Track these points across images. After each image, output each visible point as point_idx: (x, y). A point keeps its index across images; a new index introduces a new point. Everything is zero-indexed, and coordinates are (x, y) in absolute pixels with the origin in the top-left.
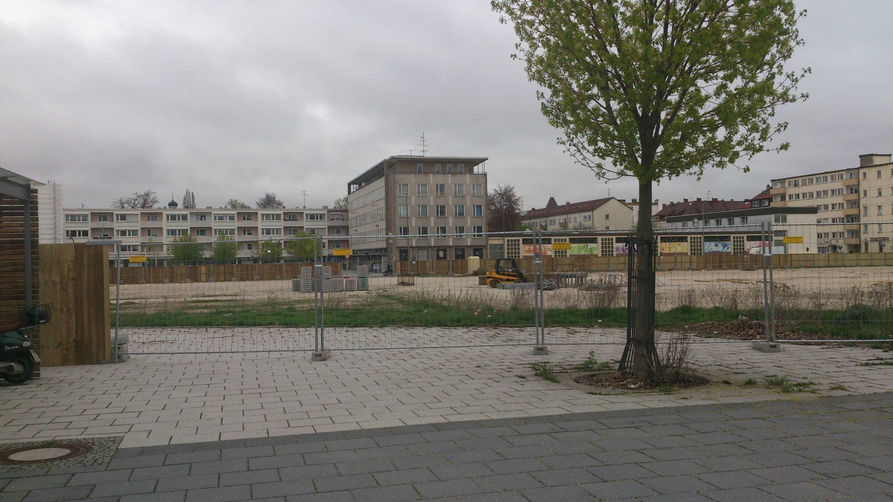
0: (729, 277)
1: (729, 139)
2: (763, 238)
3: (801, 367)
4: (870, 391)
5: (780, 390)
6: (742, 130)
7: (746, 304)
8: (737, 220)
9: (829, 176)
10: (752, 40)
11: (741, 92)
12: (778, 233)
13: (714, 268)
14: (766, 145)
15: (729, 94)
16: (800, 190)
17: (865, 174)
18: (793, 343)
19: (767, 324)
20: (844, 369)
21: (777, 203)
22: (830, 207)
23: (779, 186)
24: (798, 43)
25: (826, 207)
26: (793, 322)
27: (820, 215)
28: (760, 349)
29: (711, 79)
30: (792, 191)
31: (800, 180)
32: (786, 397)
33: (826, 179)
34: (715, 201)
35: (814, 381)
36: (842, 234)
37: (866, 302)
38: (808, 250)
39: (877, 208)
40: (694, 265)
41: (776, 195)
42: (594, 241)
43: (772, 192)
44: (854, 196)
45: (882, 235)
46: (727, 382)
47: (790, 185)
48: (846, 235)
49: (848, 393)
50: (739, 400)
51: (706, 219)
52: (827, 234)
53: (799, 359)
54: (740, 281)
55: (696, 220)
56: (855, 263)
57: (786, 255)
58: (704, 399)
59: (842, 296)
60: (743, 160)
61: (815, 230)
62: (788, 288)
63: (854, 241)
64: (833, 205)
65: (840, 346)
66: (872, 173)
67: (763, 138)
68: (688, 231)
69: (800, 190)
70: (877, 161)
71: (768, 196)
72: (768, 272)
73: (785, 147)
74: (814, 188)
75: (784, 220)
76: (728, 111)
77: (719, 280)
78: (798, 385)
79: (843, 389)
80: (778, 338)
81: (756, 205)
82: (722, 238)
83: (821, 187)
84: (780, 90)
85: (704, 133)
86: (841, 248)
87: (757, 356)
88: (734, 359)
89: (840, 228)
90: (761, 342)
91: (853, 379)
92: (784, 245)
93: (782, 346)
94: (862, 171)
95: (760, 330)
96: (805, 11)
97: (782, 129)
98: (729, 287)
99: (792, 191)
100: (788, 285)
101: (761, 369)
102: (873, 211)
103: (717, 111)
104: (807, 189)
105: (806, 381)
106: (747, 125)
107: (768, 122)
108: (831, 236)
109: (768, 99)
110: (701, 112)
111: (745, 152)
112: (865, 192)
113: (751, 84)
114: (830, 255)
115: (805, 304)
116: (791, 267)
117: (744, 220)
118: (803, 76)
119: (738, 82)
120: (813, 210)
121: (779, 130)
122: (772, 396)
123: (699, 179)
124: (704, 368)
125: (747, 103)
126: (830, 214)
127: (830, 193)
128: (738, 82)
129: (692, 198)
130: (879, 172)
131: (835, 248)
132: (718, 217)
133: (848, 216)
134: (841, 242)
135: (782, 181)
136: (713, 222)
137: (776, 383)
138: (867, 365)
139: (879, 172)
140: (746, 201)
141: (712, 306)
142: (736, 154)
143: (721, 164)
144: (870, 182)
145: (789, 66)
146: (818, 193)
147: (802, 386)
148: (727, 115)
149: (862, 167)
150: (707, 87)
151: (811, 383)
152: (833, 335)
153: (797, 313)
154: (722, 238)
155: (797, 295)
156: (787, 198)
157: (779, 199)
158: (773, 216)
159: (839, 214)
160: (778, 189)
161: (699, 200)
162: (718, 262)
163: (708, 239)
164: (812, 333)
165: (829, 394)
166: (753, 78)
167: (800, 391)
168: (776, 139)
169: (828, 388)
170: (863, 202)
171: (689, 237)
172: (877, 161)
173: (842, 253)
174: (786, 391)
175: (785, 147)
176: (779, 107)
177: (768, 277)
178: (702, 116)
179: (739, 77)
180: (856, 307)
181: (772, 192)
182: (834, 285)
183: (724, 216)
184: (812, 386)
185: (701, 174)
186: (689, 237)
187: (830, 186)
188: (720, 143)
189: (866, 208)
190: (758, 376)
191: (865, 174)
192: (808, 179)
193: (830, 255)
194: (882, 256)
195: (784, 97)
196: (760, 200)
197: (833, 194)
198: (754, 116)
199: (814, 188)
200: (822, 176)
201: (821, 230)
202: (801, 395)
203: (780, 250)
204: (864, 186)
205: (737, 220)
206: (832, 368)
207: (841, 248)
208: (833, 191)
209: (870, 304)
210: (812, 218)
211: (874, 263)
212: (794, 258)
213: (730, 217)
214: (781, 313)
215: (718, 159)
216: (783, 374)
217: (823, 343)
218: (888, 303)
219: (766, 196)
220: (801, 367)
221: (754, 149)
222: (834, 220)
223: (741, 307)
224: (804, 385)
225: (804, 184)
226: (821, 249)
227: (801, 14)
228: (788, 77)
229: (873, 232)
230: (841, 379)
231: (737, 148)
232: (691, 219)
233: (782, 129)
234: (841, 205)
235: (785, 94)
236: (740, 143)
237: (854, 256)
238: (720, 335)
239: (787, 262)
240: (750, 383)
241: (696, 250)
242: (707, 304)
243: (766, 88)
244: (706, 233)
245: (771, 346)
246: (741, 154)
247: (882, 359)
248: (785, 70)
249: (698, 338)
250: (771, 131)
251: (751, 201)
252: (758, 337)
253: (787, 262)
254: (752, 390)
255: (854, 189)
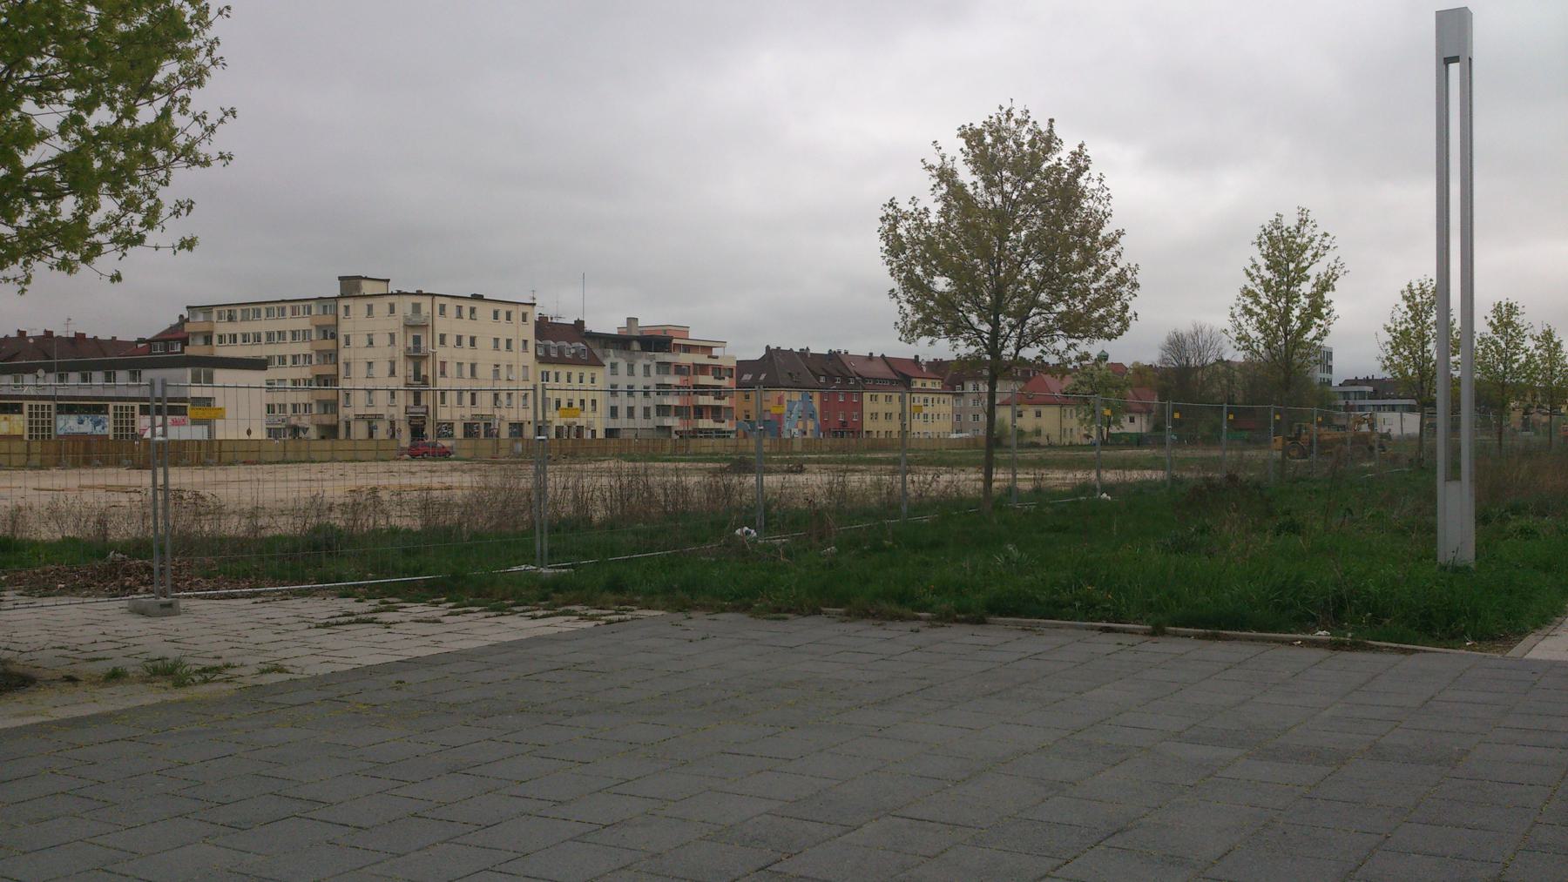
0: (100, 481)
1: (81, 219)
2: (153, 409)
3: (215, 638)
4: (326, 669)
5: (169, 684)
6: (108, 205)
7: (123, 530)
8: (122, 376)
9: (288, 306)
10: (126, 39)
11: (105, 133)
12: (197, 401)
13: (76, 465)
14: (152, 236)
15: (84, 134)
16: (239, 328)
17: (347, 308)
18: (204, 598)
19: (156, 566)
20: (288, 636)
21: (196, 349)
22: (289, 361)
23: (201, 318)
24: (214, 63)
25: (283, 360)
26: (207, 560)
27: (272, 373)
28: (142, 612)
29: (49, 101)
30: (224, 328)
31: (238, 309)
32: (180, 694)
33: (283, 312)
34: (80, 337)
35: (232, 661)
36: (308, 407)
37: (338, 521)
38: (249, 432)
39: (365, 366)
40: (36, 460)
41: (195, 334)
42: (16, 409)
43: (188, 328)
44: (328, 345)
45: (371, 411)
46: (71, 679)
47: (220, 317)
48: (314, 407)
49: (287, 677)
50: (77, 712)
51: (63, 371)
52: (283, 407)
53: (213, 625)
54: (124, 490)
55: (41, 373)
56: (327, 456)
57: (211, 441)
58: (20, 715)
59: (294, 512)
60: (108, 260)
61: (261, 399)
62: (203, 498)
63: (327, 420)
64: (294, 357)
65: (285, 596)
66: (358, 307)
67: (149, 223)
68: (25, 392)
69: (239, 328)
70: (367, 288)
71: (180, 335)
72: (160, 471)
73: (188, 244)
74: (262, 326)
75: (210, 379)
76: (80, 165)
77: (81, 488)
78: (204, 670)
79: (281, 670)
80: (179, 590)
81: (159, 350)
82: (95, 408)
83: (275, 325)
84: (180, 140)
85: (33, 202)
86: (306, 430)
87: (137, 624)
88: (92, 632)
89: (303, 397)
90: (143, 598)
91: (298, 652)
92: (207, 422)
93: (183, 604)
94: (342, 303)
95: (146, 578)
96: (228, 8)
97: (183, 212)
98: (103, 499)
99: (224, 328)
100: (202, 493)
101: (140, 649)
102: (359, 370)
103: (61, 162)
104: (251, 327)
105: (219, 663)
106: (117, 196)
107: (159, 195)
108: (289, 409)
109: (160, 155)
110: (27, 160)
111: (112, 246)
112: (347, 338)
113: (126, 123)
114: (287, 442)
115: (234, 526)
116: (220, 463)
117: (135, 376)
118: (222, 121)
119: (102, 116)
120: (260, 364)
121: (177, 213)
122: (150, 696)
123: (23, 291)
124: (26, 656)
125: (121, 156)
126: (289, 373)
127: (289, 337)
128: (102, 116)
129: (35, 330)
130: (370, 307)
131: (295, 430)
132: (85, 370)
133: (318, 377)
134: (305, 421)
135: (207, 309)
136: (74, 378)
137: (166, 672)
138: (326, 625)
139: (370, 307)
140: (141, 341)
141: (59, 536)
142: (96, 249)
143: (65, 265)
144: (355, 321)
145: (200, 99)
146: (270, 336)
147: (209, 673)
148: (76, 173)
149: (342, 297)
150: (48, 117)
151: (228, 666)
152: (278, 579)
153: (217, 544)
154: (95, 408)
155: (218, 511)
156: (215, 340)
157: (200, 342)
158: (189, 372)
159: (305, 373)
160: (198, 323)
161: (49, 334)
162: (85, 453)
163: (69, 410)
164: (236, 578)
165: (256, 682)
166: (129, 112)
167: (206, 681)
168: (170, 230)
169: (255, 671)
170: (344, 354)
171: (26, 404)
172: (367, 288)
173: (308, 440)
174: (180, 683)
175: (188, 244)
176: (180, 172)
177: (160, 481)
178: (30, 169)
179: (104, 107)
180: (317, 529)
181: (188, 328)
182: (279, 494)
183: (98, 366)
184: (231, 672)
185: (28, 281)
186: (26, 404)
187: (288, 324)
188: (65, 224)
189: (347, 365)
190: (133, 661)
191: (347, 308)
192: (252, 309)
193: (287, 442)
194: (373, 445)
195: (189, 155)
196: (166, 341)
197: (294, 338)
198: (134, 181)
199: (262, 326)
200: (277, 307)
201: (278, 398)
202: (207, 688)
203: (199, 433)
204: (345, 327)
205: (122, 376)
206: (266, 636)
207: (306, 430)
208: (294, 333)
209: (343, 524)
210: (257, 377)
211: (359, 455)
212: (225, 447)
213: (110, 369)
214: (188, 545)
215: (59, 255)
216: (177, 654)
217: (258, 594)
218: (371, 521)
219: (176, 335)
220: (215, 638)
221: (130, 240)
222: (295, 382)
223: (114, 536)
224: (217, 670)
225: (245, 319)
226: (273, 432)
227: (220, 13)
228: (196, 119)
229: (359, 404)
230: (281, 654)
231: (99, 238)
232: (31, 369)
233: (183, 212)
234: (308, 357)
235: (188, 149)
236: (103, 229)
237: (327, 444)
238: (72, 590)
239: (211, 454)
240: (116, 676)
241: (41, 429)
242: (47, 533)
243: (159, 133)
244: (60, 398)
245: (163, 606)
246: (105, 248)
247: (352, 614)
248: (195, 107)
249: (24, 599)
250: (165, 212)
251: (149, 342)
252: (142, 589)
253: (211, 454)
254: (118, 688)
255: (330, 332)
